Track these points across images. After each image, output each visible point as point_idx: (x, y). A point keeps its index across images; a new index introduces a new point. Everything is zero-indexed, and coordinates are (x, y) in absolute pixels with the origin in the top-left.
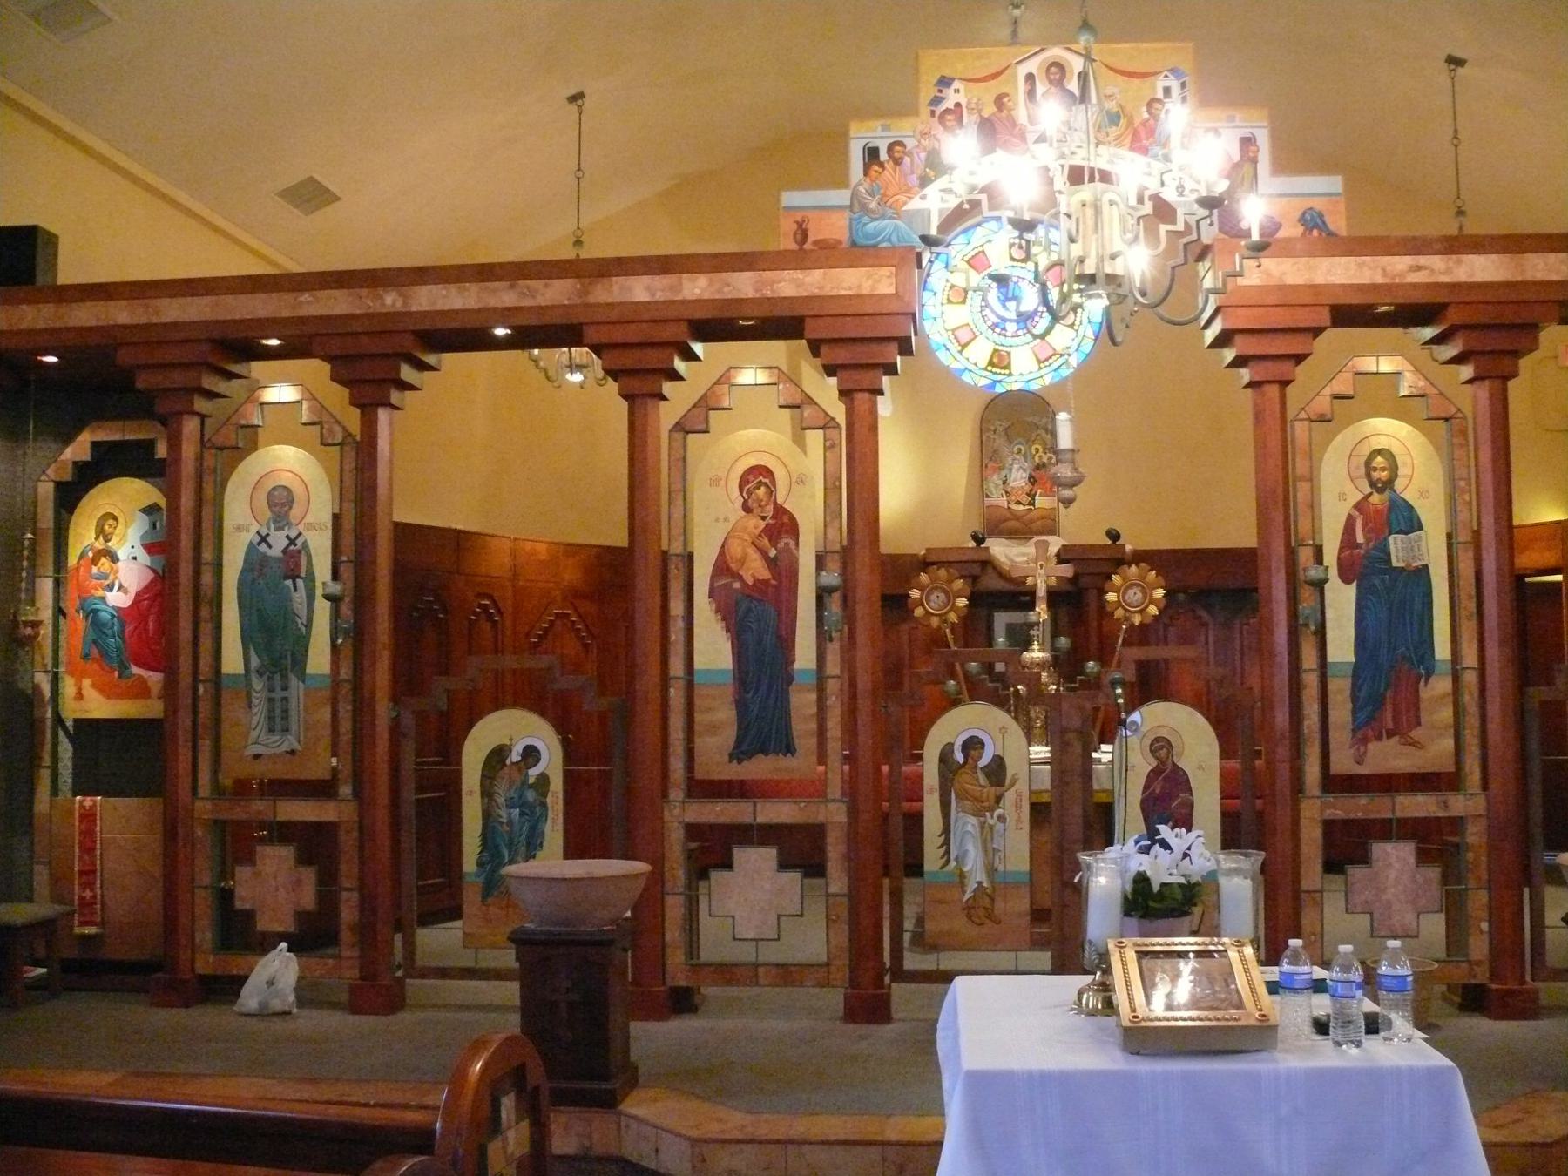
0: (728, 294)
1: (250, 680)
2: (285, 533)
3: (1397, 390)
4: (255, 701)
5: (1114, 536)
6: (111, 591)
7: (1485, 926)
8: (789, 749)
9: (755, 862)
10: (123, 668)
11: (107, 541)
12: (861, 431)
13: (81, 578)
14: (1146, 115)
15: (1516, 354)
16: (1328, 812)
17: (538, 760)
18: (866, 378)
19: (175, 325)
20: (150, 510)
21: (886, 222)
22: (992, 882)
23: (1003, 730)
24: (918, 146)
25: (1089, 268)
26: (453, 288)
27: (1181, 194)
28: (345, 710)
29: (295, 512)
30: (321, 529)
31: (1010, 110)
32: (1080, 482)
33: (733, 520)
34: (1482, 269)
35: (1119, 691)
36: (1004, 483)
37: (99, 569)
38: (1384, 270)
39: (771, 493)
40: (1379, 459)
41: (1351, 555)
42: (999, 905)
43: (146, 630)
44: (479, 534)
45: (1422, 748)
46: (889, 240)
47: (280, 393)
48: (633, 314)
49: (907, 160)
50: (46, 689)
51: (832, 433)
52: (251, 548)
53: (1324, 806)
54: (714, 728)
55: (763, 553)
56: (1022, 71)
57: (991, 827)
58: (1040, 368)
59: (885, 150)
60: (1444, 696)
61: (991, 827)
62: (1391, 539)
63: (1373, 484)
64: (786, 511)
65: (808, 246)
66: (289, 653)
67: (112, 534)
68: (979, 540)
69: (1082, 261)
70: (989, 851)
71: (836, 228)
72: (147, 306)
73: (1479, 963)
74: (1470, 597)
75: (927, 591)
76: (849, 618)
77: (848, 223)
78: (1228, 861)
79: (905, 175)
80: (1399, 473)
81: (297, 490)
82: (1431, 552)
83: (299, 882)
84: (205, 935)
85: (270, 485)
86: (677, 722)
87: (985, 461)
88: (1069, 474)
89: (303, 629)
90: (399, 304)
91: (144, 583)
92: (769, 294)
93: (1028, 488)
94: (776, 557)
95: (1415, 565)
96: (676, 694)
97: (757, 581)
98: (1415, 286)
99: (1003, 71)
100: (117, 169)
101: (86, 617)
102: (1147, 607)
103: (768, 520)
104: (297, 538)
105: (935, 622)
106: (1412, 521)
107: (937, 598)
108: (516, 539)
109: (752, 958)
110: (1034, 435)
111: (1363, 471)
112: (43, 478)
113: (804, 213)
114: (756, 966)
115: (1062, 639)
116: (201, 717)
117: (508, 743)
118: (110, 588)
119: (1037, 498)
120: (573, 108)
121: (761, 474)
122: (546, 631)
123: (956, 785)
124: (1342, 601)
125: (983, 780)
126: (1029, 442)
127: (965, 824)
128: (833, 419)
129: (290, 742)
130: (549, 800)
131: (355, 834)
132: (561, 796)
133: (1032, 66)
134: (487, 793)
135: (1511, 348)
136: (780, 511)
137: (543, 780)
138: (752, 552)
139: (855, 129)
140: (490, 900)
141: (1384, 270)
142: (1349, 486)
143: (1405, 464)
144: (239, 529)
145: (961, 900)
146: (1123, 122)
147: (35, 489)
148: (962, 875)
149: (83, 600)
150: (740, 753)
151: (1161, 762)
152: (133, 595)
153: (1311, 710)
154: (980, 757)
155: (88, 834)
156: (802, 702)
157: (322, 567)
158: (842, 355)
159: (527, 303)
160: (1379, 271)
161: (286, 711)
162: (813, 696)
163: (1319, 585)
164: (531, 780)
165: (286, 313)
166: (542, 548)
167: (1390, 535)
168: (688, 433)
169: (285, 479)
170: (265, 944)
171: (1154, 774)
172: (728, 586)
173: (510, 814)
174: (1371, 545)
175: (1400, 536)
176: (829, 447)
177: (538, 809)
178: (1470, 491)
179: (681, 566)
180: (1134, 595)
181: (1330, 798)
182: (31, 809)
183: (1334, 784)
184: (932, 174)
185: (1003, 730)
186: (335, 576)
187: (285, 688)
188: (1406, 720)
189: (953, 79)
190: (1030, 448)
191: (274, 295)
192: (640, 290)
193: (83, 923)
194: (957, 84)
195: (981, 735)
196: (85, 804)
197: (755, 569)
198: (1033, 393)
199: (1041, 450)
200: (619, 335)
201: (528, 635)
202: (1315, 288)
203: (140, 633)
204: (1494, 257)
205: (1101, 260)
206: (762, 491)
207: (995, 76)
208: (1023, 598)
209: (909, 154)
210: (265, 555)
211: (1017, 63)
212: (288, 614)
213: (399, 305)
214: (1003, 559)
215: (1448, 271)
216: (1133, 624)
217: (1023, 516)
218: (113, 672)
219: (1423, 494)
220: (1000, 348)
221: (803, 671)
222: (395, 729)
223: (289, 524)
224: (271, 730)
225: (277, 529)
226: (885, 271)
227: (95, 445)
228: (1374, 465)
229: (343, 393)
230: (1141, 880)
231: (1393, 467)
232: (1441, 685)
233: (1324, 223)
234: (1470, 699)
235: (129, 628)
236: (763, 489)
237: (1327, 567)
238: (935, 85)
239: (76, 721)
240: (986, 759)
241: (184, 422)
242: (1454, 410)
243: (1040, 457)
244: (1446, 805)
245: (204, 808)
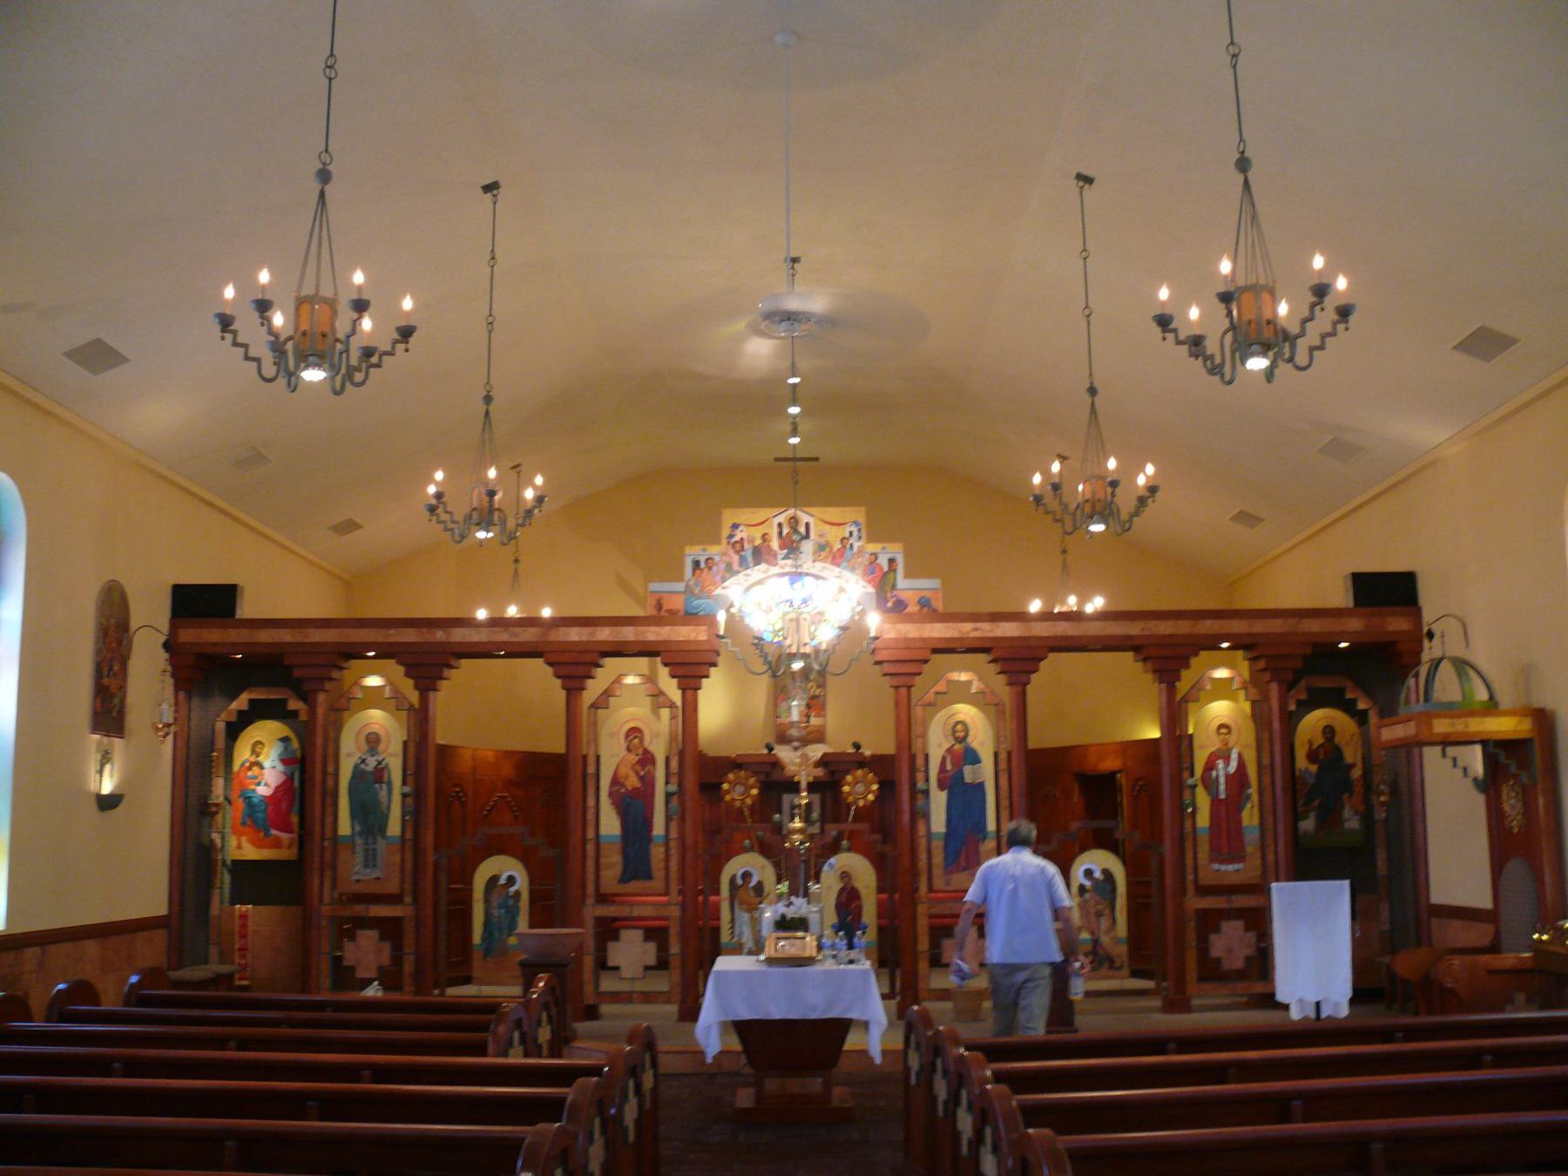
0: (620, 638)
5: (857, 746)
8: (649, 877)
10: (267, 834)
11: (258, 756)
19: (317, 643)
20: (285, 740)
23: (763, 867)
28: (409, 855)
29: (381, 747)
33: (621, 756)
39: (641, 741)
44: (459, 747)
49: (715, 568)
50: (218, 842)
52: (356, 766)
55: (637, 773)
65: (663, 613)
71: (677, 603)
75: (733, 784)
76: (682, 804)
86: (590, 863)
91: (280, 781)
96: (590, 847)
98: (973, 638)
99: (764, 522)
100: (235, 519)
105: (738, 804)
107: (739, 789)
108: (476, 749)
111: (950, 732)
112: (218, 719)
118: (259, 784)
120: (514, 473)
122: (493, 806)
124: (938, 802)
125: (752, 893)
129: (377, 873)
134: (487, 900)
136: (646, 752)
137: (518, 894)
139: (688, 550)
140: (488, 959)
144: (349, 755)
147: (214, 725)
149: (243, 791)
150: (625, 878)
153: (923, 858)
155: (244, 926)
156: (657, 852)
157: (396, 775)
158: (681, 671)
159: (514, 639)
163: (926, 793)
166: (490, 753)
168: (598, 708)
169: (375, 728)
171: (842, 890)
172: (618, 791)
176: (673, 718)
180: (860, 788)
185: (763, 867)
186: (404, 782)
187: (375, 843)
193: (241, 979)
194: (741, 528)
197: (633, 782)
202: (924, 640)
206: (637, 740)
209: (716, 564)
212: (377, 803)
213: (443, 639)
215: (992, 631)
219: (982, 744)
222: (436, 865)
223: (377, 753)
224: (366, 866)
226: (703, 628)
227: (252, 702)
229: (410, 682)
230: (783, 916)
231: (966, 730)
235: (270, 808)
239: (233, 861)
240: (753, 883)
245: (326, 910)
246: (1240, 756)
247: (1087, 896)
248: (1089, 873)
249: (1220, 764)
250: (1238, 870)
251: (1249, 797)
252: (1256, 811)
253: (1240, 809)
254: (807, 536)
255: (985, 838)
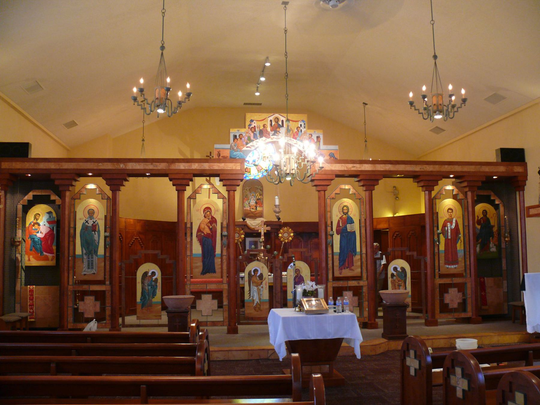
0: (202, 168)
1: (83, 256)
2: (93, 220)
3: (349, 192)
4: (84, 261)
6: (38, 233)
7: (367, 309)
9: (207, 298)
10: (41, 253)
11: (37, 220)
12: (231, 199)
13: (30, 230)
14: (296, 130)
15: (374, 185)
16: (334, 285)
17: (155, 275)
18: (233, 188)
21: (238, 152)
22: (260, 302)
23: (263, 267)
24: (245, 135)
25: (288, 172)
26: (137, 164)
27: (303, 149)
28: (108, 263)
29: (95, 216)
30: (102, 220)
31: (266, 128)
32: (280, 212)
34: (367, 167)
35: (294, 258)
36: (249, 204)
37: (35, 228)
38: (347, 167)
39: (210, 213)
40: (345, 208)
41: (339, 229)
42: (262, 307)
43: (48, 243)
45: (354, 271)
46: (239, 157)
47: (91, 186)
48: (180, 172)
49: (243, 138)
50: (19, 258)
51: (225, 200)
52: (83, 224)
53: (333, 284)
54: (197, 267)
55: (209, 227)
56: (269, 119)
57: (260, 289)
58: (258, 173)
59: (238, 136)
60: (359, 259)
61: (260, 289)
62: (347, 225)
63: (344, 213)
64: (214, 218)
65: (220, 157)
66: (93, 250)
67: (38, 219)
68: (244, 219)
69: (286, 170)
70: (259, 295)
71: (226, 153)
72: (59, 164)
73: (366, 318)
74: (364, 238)
77: (229, 153)
78: (319, 286)
79: (243, 142)
80: (349, 211)
81: (96, 210)
82: (356, 228)
83: (95, 305)
84: (71, 319)
85: (88, 209)
87: (244, 197)
88: (278, 210)
89: (97, 244)
90: (124, 167)
91: (47, 231)
92: (212, 168)
93: (255, 205)
94: (212, 228)
95: (352, 231)
97: (207, 234)
99: (265, 119)
101: (31, 240)
102: (289, 238)
103: (210, 220)
104: (95, 221)
106: (352, 221)
108: (126, 218)
109: (206, 320)
110: (257, 191)
111: (341, 210)
112: (19, 204)
113: (219, 150)
114: (207, 322)
115: (268, 246)
116: (70, 265)
117: (148, 271)
118: (38, 232)
119: (257, 207)
121: (208, 209)
123: (252, 280)
124: (337, 239)
125: (258, 279)
126: (255, 192)
127: (254, 288)
128: (225, 197)
129: (94, 271)
130: (158, 284)
131: (110, 293)
132: (161, 283)
133: (271, 118)
135: (373, 184)
136: (213, 217)
137: (156, 279)
138: (206, 226)
140: (143, 308)
141: (347, 167)
142: (338, 214)
143: (350, 209)
144: (80, 219)
145: (253, 306)
146: (291, 132)
148: (253, 300)
150: (204, 273)
151: (298, 274)
152: (44, 234)
153: (330, 262)
154: (257, 273)
156: (218, 261)
158: (228, 183)
160: (346, 167)
161: (92, 263)
162: (220, 260)
163: (332, 236)
164: (154, 280)
165: (95, 168)
166: (132, 221)
167: (347, 224)
168: (191, 199)
169: (92, 207)
170: (89, 320)
173: (148, 288)
174: (343, 226)
175: (349, 225)
177: (155, 286)
178: (364, 215)
179: (190, 230)
180: (286, 235)
181: (334, 282)
182: (15, 289)
183: (335, 279)
184: (249, 142)
185: (263, 267)
186: (105, 231)
187: (92, 258)
188: (350, 265)
189: (254, 120)
190: (256, 194)
191: (92, 163)
192: (182, 166)
193: (30, 318)
194: (254, 121)
195: (258, 268)
196: (30, 288)
197: (207, 231)
198: (256, 179)
199: (259, 195)
200: (176, 177)
201: (129, 244)
202: (332, 171)
203: (46, 244)
204: (370, 165)
205: (290, 170)
207: (263, 120)
208: (254, 234)
209: (244, 137)
210: (87, 226)
211: (268, 117)
214: (249, 224)
216: (285, 242)
217: (254, 212)
218: (38, 254)
219: (354, 215)
220: (248, 167)
221: (218, 254)
222: (121, 268)
223: (93, 218)
224: (89, 268)
225: (90, 219)
226: (238, 164)
227: (34, 196)
228: (344, 209)
231: (348, 209)
232: (358, 257)
233: (334, 156)
234: (364, 260)
235: (43, 243)
236: (209, 212)
237: (334, 232)
238: (250, 121)
241: (66, 193)
242: (361, 197)
243: (258, 197)
244: (359, 283)
245: (70, 288)
246: (456, 221)
247: (395, 278)
248: (395, 269)
249: (449, 224)
250: (455, 268)
251: (460, 238)
252: (462, 243)
253: (456, 243)
254: (283, 126)
255: (355, 255)
